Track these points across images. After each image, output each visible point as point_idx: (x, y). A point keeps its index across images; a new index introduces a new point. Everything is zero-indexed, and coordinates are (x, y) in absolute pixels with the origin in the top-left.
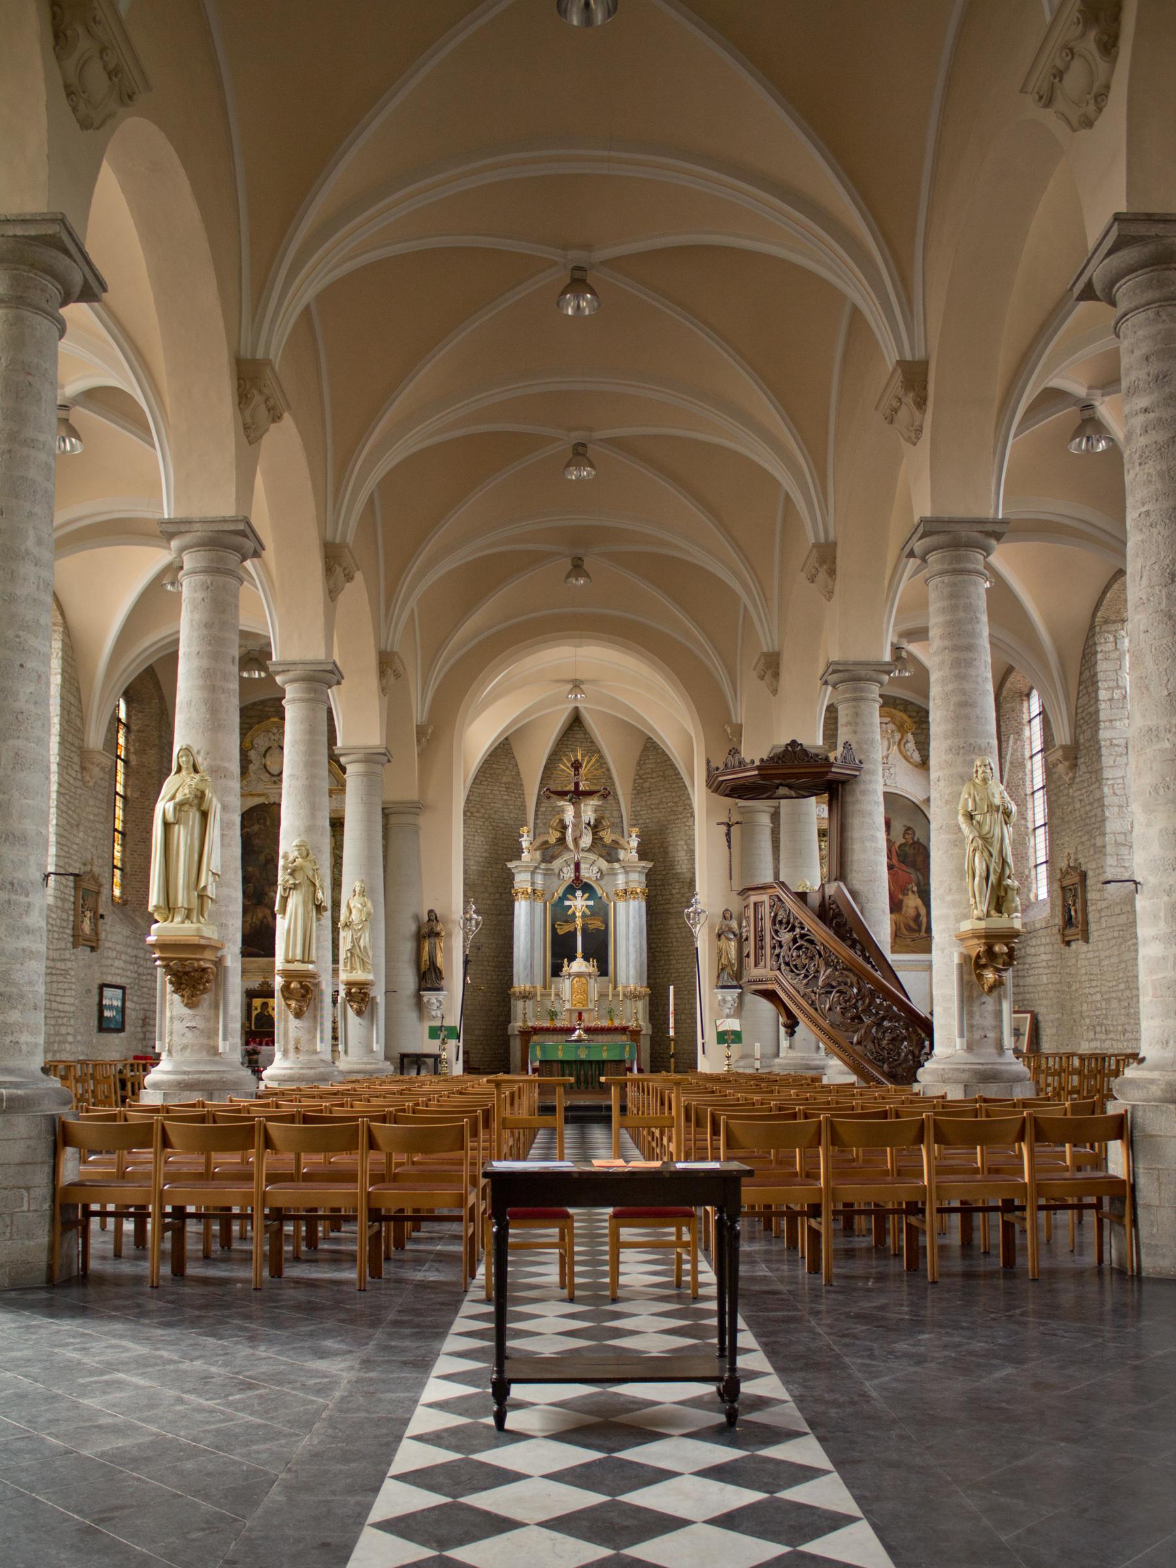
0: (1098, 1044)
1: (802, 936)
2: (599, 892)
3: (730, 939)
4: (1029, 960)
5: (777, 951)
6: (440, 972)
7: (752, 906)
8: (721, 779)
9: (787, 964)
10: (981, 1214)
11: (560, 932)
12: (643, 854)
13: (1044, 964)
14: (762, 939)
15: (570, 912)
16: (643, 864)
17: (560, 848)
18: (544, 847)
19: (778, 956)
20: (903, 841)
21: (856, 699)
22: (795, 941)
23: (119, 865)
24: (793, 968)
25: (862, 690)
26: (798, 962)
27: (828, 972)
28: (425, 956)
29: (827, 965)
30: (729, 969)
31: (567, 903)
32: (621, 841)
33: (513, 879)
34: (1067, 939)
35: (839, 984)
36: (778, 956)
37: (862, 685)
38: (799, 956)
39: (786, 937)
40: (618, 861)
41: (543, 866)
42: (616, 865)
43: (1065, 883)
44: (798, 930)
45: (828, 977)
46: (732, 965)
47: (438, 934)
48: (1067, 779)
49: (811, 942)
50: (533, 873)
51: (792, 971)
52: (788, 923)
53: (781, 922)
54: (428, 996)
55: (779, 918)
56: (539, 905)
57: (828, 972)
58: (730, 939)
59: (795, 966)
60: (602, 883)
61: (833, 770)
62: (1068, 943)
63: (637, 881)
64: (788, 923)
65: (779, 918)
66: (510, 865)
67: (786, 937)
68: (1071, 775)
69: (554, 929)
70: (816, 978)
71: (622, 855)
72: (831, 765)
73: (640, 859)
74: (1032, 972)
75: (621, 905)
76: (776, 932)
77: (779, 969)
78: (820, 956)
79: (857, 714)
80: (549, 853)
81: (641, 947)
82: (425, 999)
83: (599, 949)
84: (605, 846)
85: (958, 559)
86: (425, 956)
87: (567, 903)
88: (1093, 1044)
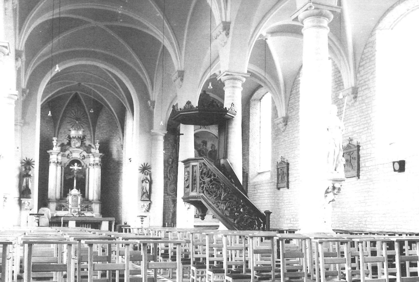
0: (292, 225)
1: (214, 179)
2: (83, 164)
3: (147, 183)
4: (258, 194)
5: (202, 186)
6: (30, 190)
7: (191, 166)
8: (181, 113)
9: (207, 191)
10: (32, 258)
11: (67, 178)
12: (101, 150)
13: (267, 196)
14: (195, 180)
15: (72, 171)
16: (101, 154)
17: (68, 147)
18: (62, 145)
19: (203, 187)
20: (211, 150)
21: (233, 87)
22: (211, 181)
23: (51, 55)
24: (209, 192)
25: (236, 84)
26: (212, 190)
27: (225, 195)
28: (24, 184)
29: (225, 192)
30: (146, 194)
31: (71, 167)
32: (93, 145)
33: (49, 157)
34: (278, 187)
35: (230, 199)
36: (203, 187)
37: (236, 81)
38: (213, 188)
39: (207, 180)
40: (91, 152)
41: (61, 153)
42: (90, 154)
43: (279, 167)
44: (213, 177)
45: (225, 197)
46: (147, 192)
47: (30, 176)
48: (282, 129)
49: (219, 182)
50: (57, 155)
51: (209, 194)
52: (208, 174)
53: (205, 174)
54: (24, 200)
55: (204, 172)
56: (59, 168)
57: (225, 195)
58: (147, 183)
59: (211, 192)
60: (84, 160)
61: (228, 113)
62: (279, 189)
63: (98, 160)
64: (208, 174)
65: (204, 172)
66: (48, 152)
67: (207, 180)
68: (284, 128)
69: (65, 177)
70: (220, 197)
71: (93, 150)
72: (227, 111)
73: (100, 152)
74: (261, 199)
75: (91, 168)
76: (203, 178)
77: (203, 192)
78: (222, 188)
79: (234, 93)
80: (63, 148)
81: (99, 185)
82: (23, 202)
83: (82, 186)
84: (86, 147)
85: (320, 22)
86: (24, 184)
87: (71, 167)
88: (289, 225)
